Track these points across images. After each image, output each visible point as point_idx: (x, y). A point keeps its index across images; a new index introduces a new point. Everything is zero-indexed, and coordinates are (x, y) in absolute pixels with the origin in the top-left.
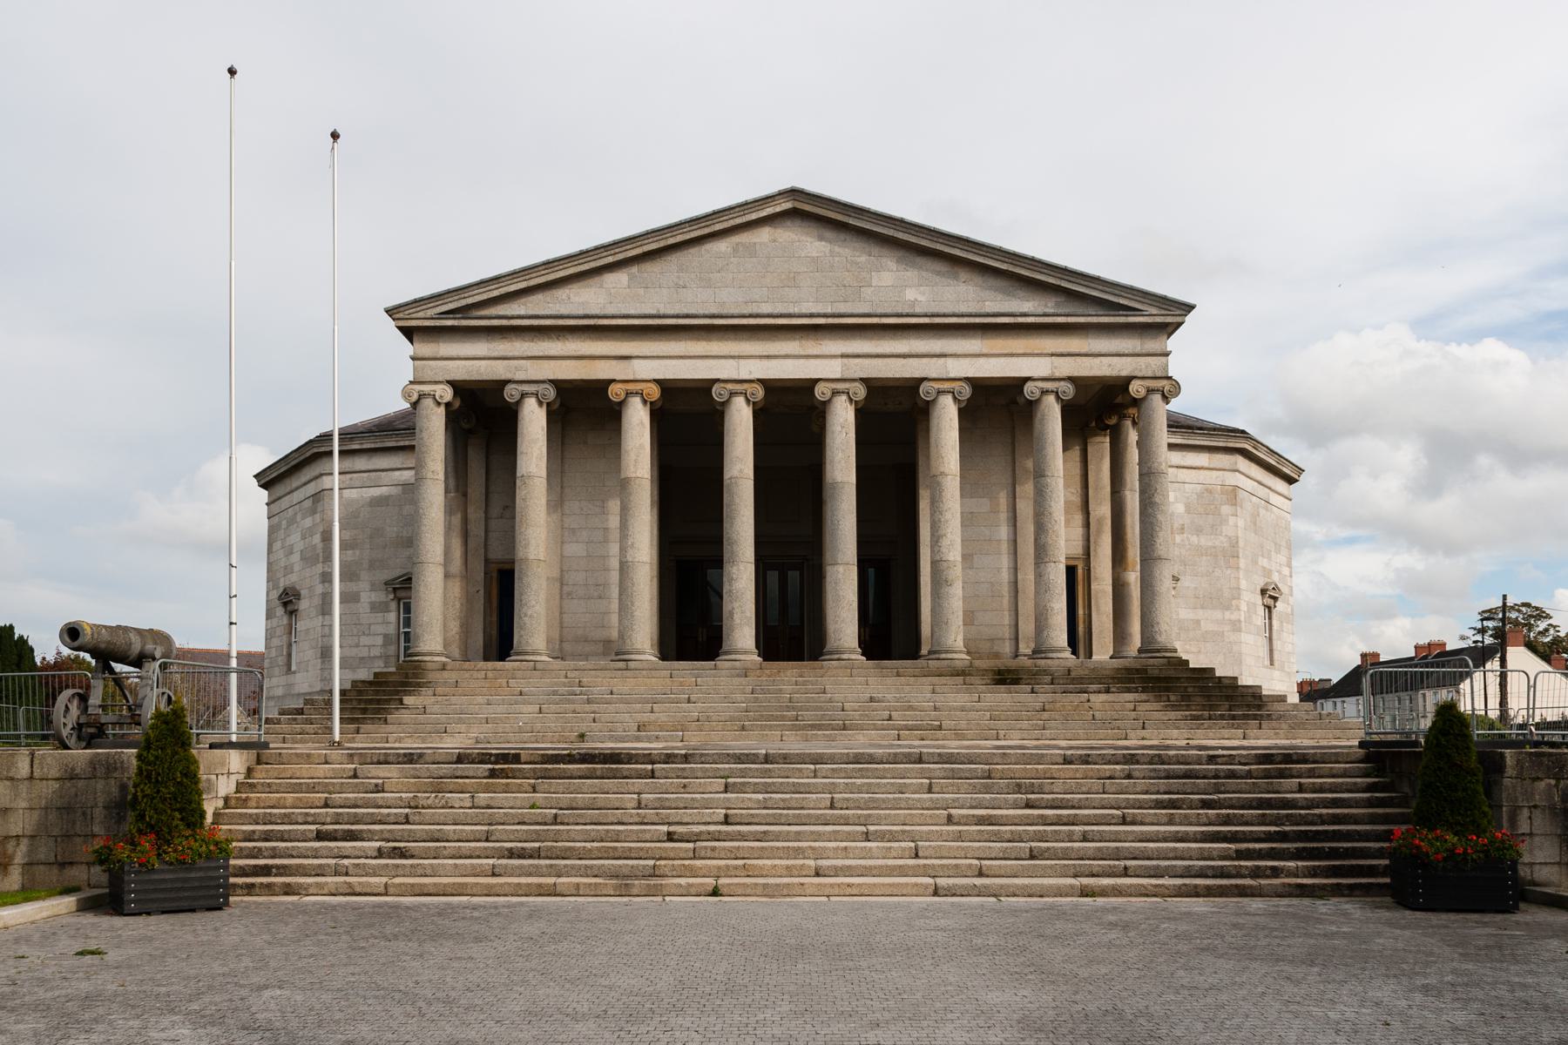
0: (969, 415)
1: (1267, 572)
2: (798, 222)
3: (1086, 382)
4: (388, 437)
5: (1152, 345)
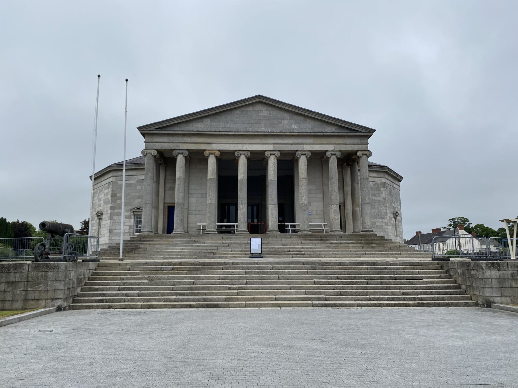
0: (310, 161)
1: (394, 208)
2: (260, 105)
3: (346, 153)
4: (134, 166)
5: (363, 142)
